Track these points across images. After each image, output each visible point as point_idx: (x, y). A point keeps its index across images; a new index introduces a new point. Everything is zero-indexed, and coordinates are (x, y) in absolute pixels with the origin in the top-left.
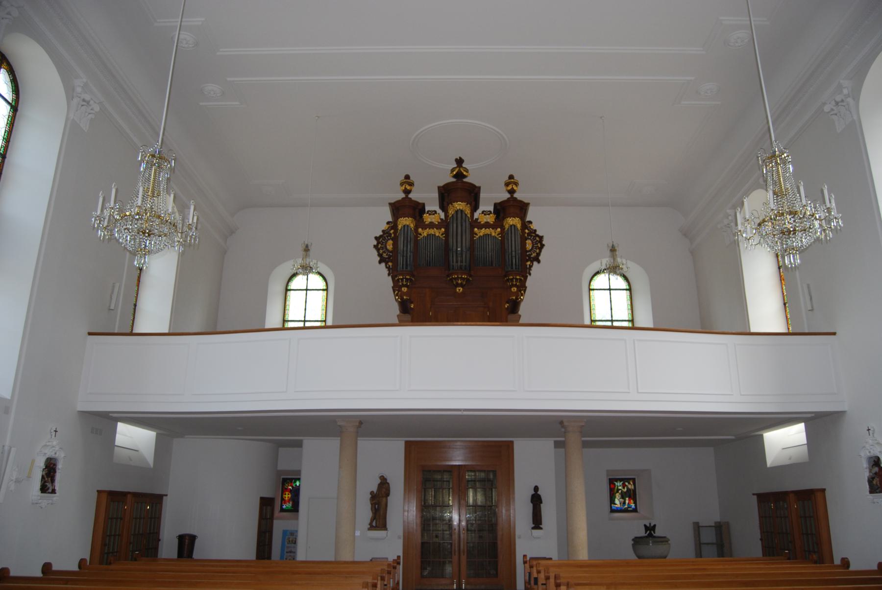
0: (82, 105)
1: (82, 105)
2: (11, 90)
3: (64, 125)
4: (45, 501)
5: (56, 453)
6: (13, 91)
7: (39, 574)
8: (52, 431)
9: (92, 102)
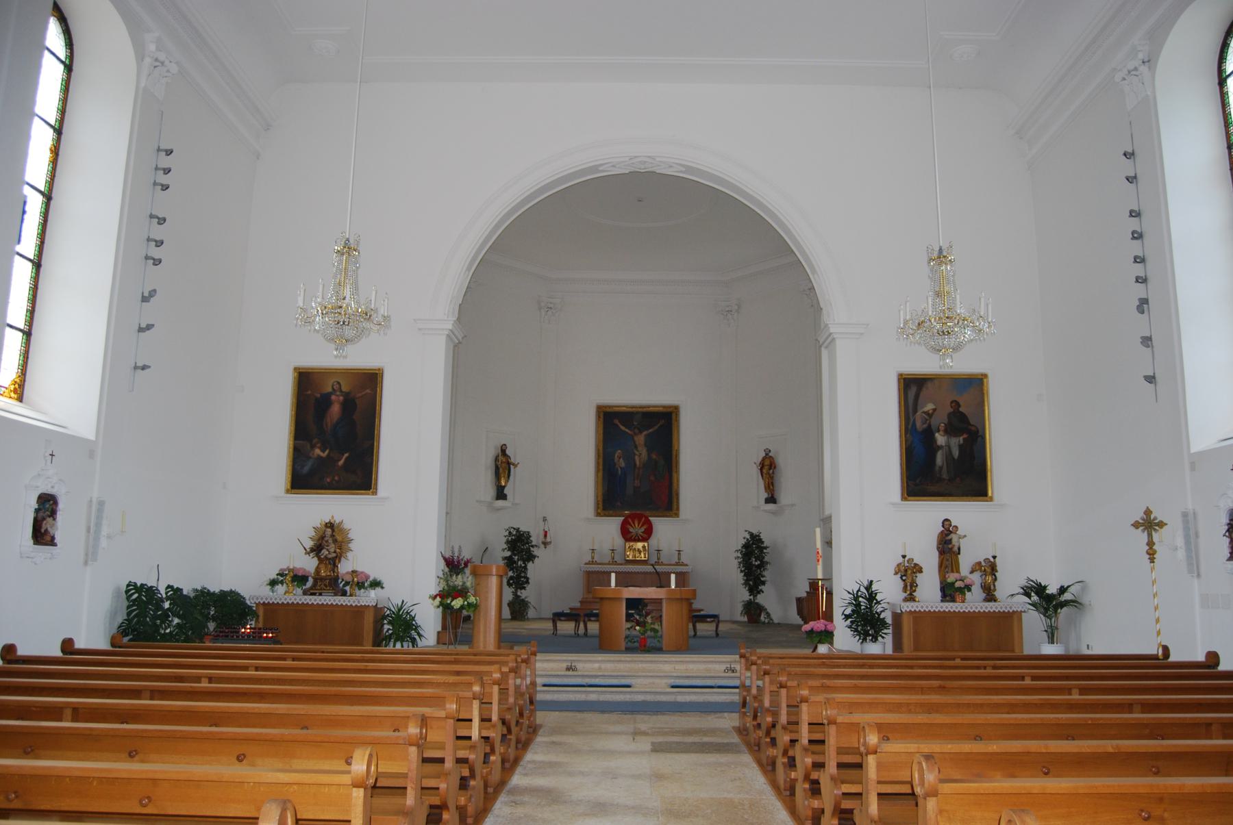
0: (155, 67)
1: (155, 67)
2: (64, 44)
3: (133, 94)
4: (41, 554)
5: (53, 487)
6: (66, 45)
7: (58, 653)
8: (47, 454)
9: (167, 62)
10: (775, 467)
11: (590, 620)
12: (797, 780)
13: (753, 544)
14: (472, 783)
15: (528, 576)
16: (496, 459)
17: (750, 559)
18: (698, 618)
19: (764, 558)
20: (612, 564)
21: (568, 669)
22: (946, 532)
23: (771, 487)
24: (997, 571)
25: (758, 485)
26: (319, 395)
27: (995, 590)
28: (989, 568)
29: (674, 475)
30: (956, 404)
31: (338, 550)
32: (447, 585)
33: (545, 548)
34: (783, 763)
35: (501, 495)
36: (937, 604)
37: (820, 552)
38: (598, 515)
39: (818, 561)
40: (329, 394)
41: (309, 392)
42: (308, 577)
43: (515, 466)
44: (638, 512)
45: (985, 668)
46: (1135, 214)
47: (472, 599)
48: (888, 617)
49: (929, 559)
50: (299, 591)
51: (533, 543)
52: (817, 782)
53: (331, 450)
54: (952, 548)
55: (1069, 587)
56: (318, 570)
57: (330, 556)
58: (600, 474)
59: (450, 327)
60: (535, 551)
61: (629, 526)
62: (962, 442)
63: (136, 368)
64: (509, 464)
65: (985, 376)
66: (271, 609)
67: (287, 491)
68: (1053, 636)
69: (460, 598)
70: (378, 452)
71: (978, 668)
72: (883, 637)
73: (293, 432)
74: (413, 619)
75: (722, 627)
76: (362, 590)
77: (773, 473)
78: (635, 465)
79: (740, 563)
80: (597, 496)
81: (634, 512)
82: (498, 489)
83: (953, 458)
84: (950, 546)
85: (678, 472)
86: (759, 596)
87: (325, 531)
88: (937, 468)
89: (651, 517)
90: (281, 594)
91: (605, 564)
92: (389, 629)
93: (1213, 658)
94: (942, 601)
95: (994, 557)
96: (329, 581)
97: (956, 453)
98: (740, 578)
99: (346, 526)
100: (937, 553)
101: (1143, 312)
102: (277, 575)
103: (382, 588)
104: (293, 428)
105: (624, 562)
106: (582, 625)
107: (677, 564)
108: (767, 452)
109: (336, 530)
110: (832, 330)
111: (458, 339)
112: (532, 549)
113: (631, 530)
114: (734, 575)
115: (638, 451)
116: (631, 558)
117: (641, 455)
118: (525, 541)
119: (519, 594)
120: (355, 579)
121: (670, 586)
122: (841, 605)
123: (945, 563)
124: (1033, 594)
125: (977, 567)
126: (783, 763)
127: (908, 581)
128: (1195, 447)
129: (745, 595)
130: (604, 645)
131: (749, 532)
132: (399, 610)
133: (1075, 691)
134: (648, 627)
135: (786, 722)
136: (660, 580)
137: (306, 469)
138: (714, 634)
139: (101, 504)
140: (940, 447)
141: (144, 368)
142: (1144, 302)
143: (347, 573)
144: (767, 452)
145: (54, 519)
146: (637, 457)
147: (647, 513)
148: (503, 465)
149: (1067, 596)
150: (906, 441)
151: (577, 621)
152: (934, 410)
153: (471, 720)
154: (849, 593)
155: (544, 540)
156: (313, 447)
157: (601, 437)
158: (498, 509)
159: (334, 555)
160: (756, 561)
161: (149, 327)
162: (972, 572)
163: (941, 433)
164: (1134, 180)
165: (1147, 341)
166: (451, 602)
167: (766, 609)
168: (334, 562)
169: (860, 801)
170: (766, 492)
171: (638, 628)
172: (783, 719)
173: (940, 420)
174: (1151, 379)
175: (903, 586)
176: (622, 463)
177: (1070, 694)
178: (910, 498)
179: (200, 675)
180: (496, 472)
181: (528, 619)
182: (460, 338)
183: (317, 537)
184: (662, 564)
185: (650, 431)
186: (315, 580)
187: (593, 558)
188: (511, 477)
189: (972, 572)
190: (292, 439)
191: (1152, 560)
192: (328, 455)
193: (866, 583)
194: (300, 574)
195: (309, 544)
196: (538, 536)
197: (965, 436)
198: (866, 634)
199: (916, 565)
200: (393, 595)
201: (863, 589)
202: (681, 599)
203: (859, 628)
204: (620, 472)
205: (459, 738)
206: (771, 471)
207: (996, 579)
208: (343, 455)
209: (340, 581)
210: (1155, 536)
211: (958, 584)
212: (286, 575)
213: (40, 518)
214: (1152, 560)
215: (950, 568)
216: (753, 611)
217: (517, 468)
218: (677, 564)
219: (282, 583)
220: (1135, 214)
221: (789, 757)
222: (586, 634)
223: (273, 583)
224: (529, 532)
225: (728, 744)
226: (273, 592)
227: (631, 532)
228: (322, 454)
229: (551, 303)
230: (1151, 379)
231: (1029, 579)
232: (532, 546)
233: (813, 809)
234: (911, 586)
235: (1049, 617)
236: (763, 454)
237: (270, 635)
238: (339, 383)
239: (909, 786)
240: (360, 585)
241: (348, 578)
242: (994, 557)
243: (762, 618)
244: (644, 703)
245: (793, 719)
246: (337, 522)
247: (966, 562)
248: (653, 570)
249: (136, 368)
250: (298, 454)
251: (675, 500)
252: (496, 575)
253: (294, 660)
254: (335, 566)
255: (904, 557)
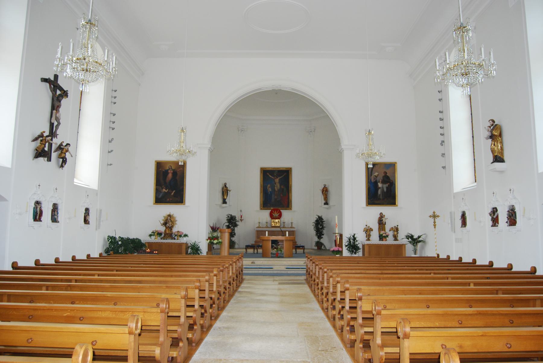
7: (34, 265)
10: (328, 191)
11: (259, 248)
12: (344, 325)
13: (319, 220)
14: (214, 306)
15: (235, 232)
16: (223, 189)
17: (318, 226)
18: (297, 247)
19: (323, 225)
20: (266, 228)
21: (252, 263)
22: (381, 217)
23: (326, 199)
24: (398, 230)
25: (321, 197)
26: (164, 170)
27: (398, 237)
28: (396, 230)
29: (290, 194)
30: (386, 173)
31: (172, 224)
32: (212, 236)
33: (241, 221)
34: (338, 318)
35: (224, 202)
36: (392, 242)
37: (337, 224)
38: (261, 209)
39: (336, 227)
40: (168, 170)
41: (161, 169)
42: (162, 233)
43: (230, 191)
44: (276, 208)
45: (448, 278)
46: (441, 112)
47: (220, 240)
48: (360, 246)
49: (375, 226)
50: (159, 238)
51: (237, 220)
52: (353, 326)
53: (169, 190)
54: (383, 222)
55: (421, 236)
56: (165, 231)
57: (170, 226)
58: (262, 194)
59: (210, 146)
60: (238, 223)
61: (273, 213)
62: (387, 186)
63: (108, 165)
64: (227, 190)
65: (396, 163)
66: (150, 244)
67: (154, 204)
68: (416, 252)
69: (216, 240)
70: (185, 190)
71: (443, 278)
72: (358, 253)
73: (155, 183)
74: (199, 247)
75: (305, 251)
76: (181, 238)
77: (327, 193)
78: (275, 190)
79: (314, 227)
80: (260, 202)
81: (275, 208)
82: (223, 200)
83: (384, 192)
84: (382, 222)
85: (291, 193)
86: (321, 239)
87: (168, 217)
88: (379, 195)
89: (281, 210)
90: (153, 239)
91: (264, 228)
92: (190, 251)
93: (534, 270)
94: (379, 241)
95: (398, 226)
96: (169, 235)
97: (385, 190)
98: (314, 233)
99: (175, 216)
100: (378, 224)
101: (442, 145)
102: (152, 233)
103: (188, 237)
104: (155, 182)
105: (271, 227)
106: (256, 250)
107: (291, 228)
108: (325, 186)
109: (171, 217)
110: (343, 147)
111: (212, 149)
112: (236, 222)
113: (274, 215)
114: (312, 232)
115: (276, 185)
116: (273, 225)
117: (277, 186)
118: (234, 219)
119: (232, 239)
120: (179, 234)
121: (286, 235)
122: (345, 242)
123: (380, 227)
124: (409, 238)
125: (391, 229)
126: (331, 308)
127: (368, 233)
128: (455, 191)
129: (316, 239)
130: (264, 255)
131: (318, 216)
132: (194, 244)
133: (472, 285)
134: (279, 249)
135: (339, 299)
136: (283, 233)
137: (160, 196)
138: (303, 252)
139: (101, 211)
140: (380, 188)
141: (111, 165)
142: (443, 142)
143: (176, 232)
144: (325, 186)
145: (89, 216)
146: (276, 187)
147: (280, 208)
148: (225, 191)
149: (420, 239)
150: (368, 186)
151: (254, 249)
152: (378, 175)
153: (205, 290)
154: (347, 238)
155: (241, 219)
156: (162, 188)
157: (262, 179)
158: (223, 208)
159: (171, 226)
160: (320, 226)
161: (112, 151)
162: (390, 231)
163: (380, 183)
164: (441, 100)
165: (443, 155)
166: (213, 241)
167: (324, 244)
168: (171, 228)
169: (373, 336)
170: (324, 200)
171: (275, 250)
172: (331, 290)
173: (380, 178)
174: (444, 167)
175: (366, 235)
176: (270, 190)
177: (469, 286)
178: (369, 205)
179: (94, 274)
180: (223, 194)
181: (235, 248)
182: (213, 149)
183: (165, 220)
184: (286, 228)
185: (281, 177)
186: (165, 234)
187: (259, 225)
188: (228, 196)
189: (390, 231)
190: (155, 186)
191: (435, 228)
192: (168, 191)
193: (353, 235)
194: (160, 232)
195: (162, 222)
196: (238, 217)
197: (389, 184)
198: (353, 252)
199: (371, 228)
200: (191, 240)
201: (352, 237)
202: (290, 240)
203: (350, 250)
204: (269, 193)
205: (188, 306)
206: (326, 193)
207: (398, 233)
208: (173, 191)
209: (173, 234)
210: (436, 220)
211: (384, 235)
212: (155, 233)
213: (85, 216)
214: (435, 228)
215: (382, 229)
216: (319, 245)
217: (230, 192)
218: (291, 228)
219: (153, 235)
220: (441, 112)
221: (333, 306)
222: (257, 253)
223: (150, 235)
224: (235, 216)
225: (301, 283)
226: (151, 238)
227: (274, 216)
228: (165, 191)
229: (243, 128)
230: (444, 167)
231: (408, 233)
232: (237, 221)
233: (351, 340)
234: (369, 236)
235: (415, 246)
236: (323, 186)
237: (156, 252)
238: (171, 166)
239: (395, 329)
240: (180, 236)
241: (176, 234)
242: (398, 226)
243: (322, 248)
244: (277, 273)
245: (343, 297)
246: (172, 214)
247: (388, 227)
248: (280, 230)
249: (108, 165)
250: (157, 191)
251: (290, 204)
252: (228, 232)
253: (99, 275)
254: (171, 229)
255: (366, 225)
